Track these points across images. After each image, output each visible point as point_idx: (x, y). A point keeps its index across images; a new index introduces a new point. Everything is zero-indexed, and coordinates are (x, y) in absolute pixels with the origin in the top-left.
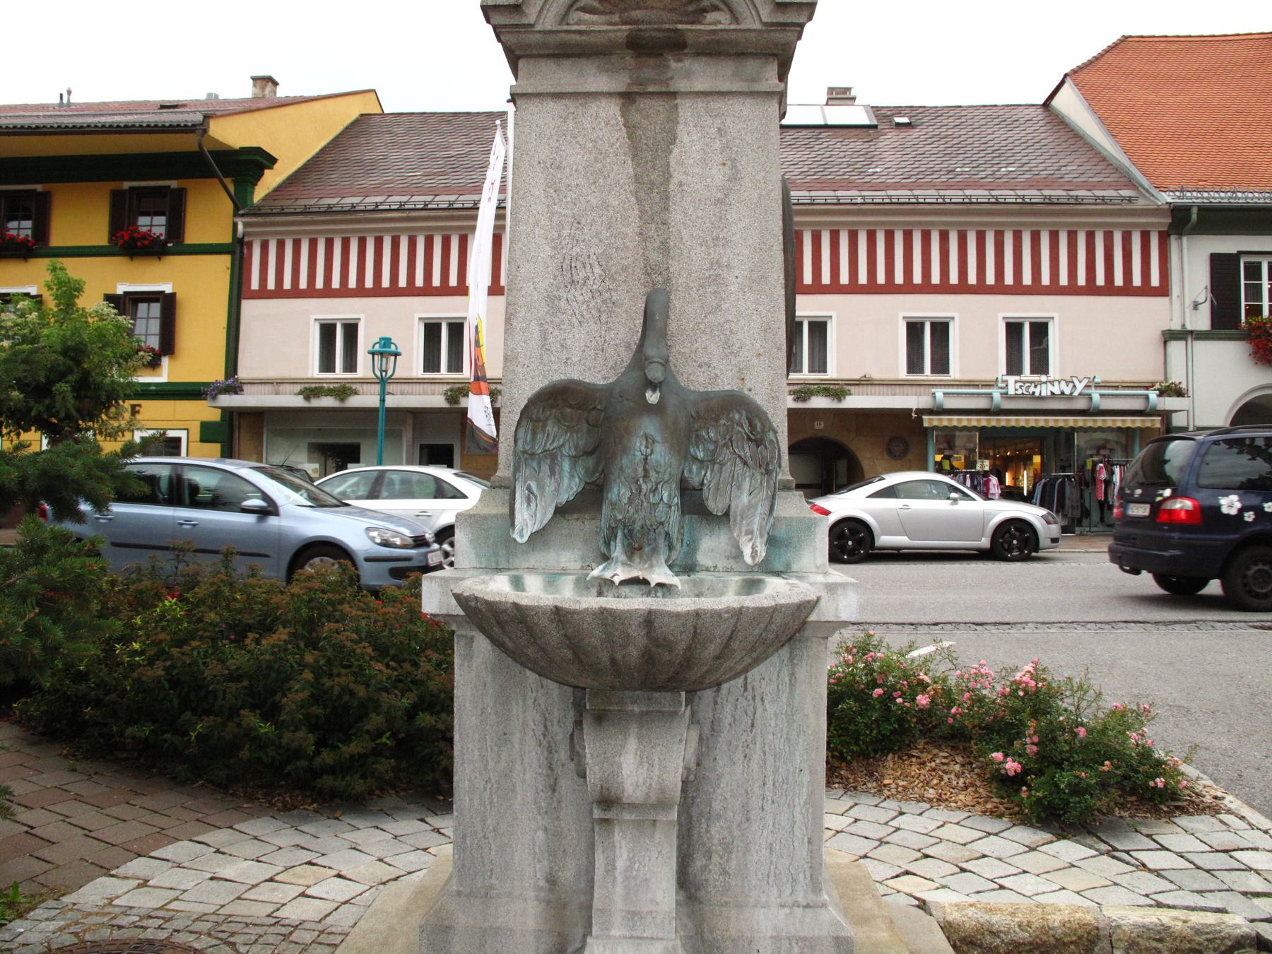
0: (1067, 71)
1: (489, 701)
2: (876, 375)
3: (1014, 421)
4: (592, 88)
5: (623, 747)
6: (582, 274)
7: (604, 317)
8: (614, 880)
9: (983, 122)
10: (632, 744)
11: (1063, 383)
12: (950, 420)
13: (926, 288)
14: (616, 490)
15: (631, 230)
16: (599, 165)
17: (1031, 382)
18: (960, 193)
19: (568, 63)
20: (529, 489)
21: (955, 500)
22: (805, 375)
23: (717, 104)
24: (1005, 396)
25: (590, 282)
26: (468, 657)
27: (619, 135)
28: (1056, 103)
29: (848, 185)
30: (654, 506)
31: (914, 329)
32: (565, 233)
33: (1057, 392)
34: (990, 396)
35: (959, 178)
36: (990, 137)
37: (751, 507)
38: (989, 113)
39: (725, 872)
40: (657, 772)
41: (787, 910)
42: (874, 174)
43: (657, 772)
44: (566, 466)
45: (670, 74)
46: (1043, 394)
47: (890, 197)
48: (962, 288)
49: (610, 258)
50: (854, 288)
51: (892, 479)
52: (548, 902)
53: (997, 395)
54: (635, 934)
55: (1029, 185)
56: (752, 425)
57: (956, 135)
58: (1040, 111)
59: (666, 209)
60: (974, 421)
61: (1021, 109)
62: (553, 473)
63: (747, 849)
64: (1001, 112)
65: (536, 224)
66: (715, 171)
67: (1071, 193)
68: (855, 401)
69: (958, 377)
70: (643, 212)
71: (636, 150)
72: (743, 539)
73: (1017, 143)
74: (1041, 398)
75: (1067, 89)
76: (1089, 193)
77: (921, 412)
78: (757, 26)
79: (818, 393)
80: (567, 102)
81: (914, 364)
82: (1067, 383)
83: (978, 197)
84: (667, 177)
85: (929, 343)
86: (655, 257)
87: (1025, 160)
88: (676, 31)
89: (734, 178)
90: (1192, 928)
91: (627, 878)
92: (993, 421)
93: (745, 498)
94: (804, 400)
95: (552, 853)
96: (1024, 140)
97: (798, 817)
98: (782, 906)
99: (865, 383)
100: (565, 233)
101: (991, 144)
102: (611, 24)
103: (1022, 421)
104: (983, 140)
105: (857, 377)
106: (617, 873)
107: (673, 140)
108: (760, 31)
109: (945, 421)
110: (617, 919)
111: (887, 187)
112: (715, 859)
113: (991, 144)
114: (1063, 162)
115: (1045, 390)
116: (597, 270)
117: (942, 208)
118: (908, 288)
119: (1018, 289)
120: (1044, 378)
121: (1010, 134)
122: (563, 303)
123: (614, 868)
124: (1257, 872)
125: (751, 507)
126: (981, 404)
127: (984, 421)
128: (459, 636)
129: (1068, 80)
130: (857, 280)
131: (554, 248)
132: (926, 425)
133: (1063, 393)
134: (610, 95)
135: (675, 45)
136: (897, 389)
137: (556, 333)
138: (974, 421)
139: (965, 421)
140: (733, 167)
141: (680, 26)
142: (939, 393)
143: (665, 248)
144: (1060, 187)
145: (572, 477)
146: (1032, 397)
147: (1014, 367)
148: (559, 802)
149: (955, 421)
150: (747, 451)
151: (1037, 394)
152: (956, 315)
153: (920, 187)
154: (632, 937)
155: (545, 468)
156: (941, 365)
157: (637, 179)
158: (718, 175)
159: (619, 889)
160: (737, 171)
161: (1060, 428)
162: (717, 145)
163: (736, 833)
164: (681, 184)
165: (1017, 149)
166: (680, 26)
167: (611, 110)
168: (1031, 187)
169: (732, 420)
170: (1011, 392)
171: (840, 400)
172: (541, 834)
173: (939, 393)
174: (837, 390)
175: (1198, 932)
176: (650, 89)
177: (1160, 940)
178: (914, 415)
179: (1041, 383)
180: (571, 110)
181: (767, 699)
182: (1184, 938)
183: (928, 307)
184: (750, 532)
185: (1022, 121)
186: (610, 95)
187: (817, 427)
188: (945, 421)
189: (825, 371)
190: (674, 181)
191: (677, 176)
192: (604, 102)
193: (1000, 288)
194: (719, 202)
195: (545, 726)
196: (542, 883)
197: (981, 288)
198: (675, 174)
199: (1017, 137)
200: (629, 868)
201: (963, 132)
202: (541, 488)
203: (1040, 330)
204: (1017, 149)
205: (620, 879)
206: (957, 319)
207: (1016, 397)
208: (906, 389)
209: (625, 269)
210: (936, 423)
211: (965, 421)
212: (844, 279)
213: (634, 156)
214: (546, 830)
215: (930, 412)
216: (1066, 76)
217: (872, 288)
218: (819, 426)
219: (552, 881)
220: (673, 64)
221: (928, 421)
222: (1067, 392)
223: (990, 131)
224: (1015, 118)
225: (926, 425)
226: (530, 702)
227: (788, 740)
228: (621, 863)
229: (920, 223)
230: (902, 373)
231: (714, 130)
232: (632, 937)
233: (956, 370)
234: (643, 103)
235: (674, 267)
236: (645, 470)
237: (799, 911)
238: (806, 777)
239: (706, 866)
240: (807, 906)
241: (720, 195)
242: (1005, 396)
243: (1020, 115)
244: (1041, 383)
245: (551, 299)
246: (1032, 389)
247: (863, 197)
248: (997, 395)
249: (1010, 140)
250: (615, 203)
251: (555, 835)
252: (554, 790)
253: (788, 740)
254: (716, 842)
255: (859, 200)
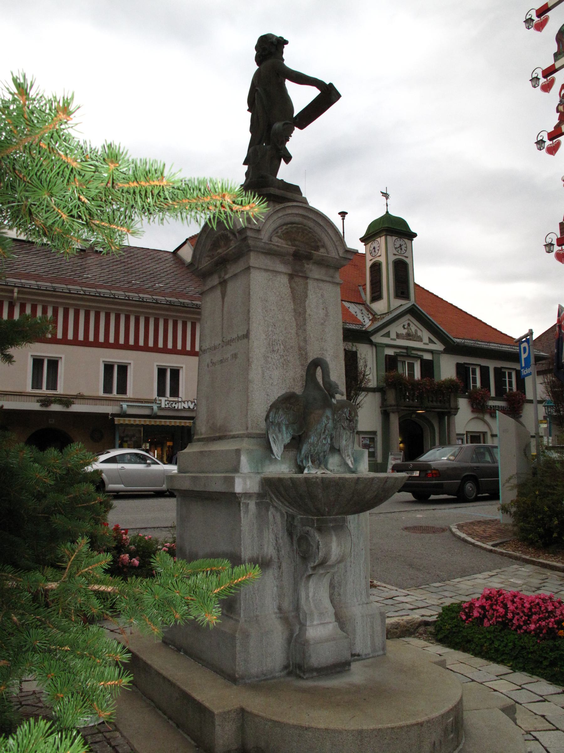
0: (188, 237)
1: (255, 531)
2: (86, 393)
3: (163, 422)
4: (280, 270)
5: (332, 540)
6: (276, 348)
7: (285, 367)
8: (310, 602)
9: (142, 257)
10: (334, 538)
11: (190, 403)
12: (135, 421)
13: (116, 346)
14: (312, 438)
15: (293, 331)
16: (281, 303)
17: (173, 401)
18: (94, 290)
19: (269, 257)
20: (273, 437)
21: (149, 465)
22: (44, 390)
23: (321, 284)
24: (160, 408)
25: (279, 351)
26: (247, 512)
27: (286, 291)
28: (180, 252)
29: (74, 283)
30: (324, 444)
31: (108, 368)
32: (270, 329)
33: (186, 407)
34: (152, 408)
35: (135, 287)
36: (148, 266)
37: (347, 446)
38: (145, 252)
39: (339, 595)
40: (343, 548)
41: (361, 606)
42: (87, 278)
43: (343, 548)
44: (284, 429)
45: (305, 269)
46: (180, 408)
47: (100, 293)
48: (136, 347)
49: (286, 342)
50: (75, 342)
51: (114, 453)
52: (281, 618)
53: (155, 407)
54: (322, 622)
55: (171, 295)
56: (350, 414)
57: (130, 262)
58: (171, 256)
59: (305, 324)
60: (142, 421)
61: (161, 253)
62: (280, 431)
63: (346, 583)
64: (151, 253)
65: (259, 324)
66: (320, 312)
67: (194, 302)
68: (77, 408)
69: (131, 397)
70: (297, 325)
71: (294, 298)
72: (347, 458)
73: (162, 271)
74: (178, 410)
75: (187, 246)
76: (177, 300)
77: (114, 415)
78: (337, 257)
79: (55, 402)
80: (269, 273)
81: (108, 388)
82: (192, 402)
83: (104, 293)
84: (305, 312)
85: (116, 376)
86: (302, 344)
87: (167, 281)
88: (311, 253)
89: (327, 315)
90: (406, 622)
91: (313, 601)
92: (152, 422)
93: (344, 443)
94: (47, 406)
95: (280, 596)
96: (165, 270)
97: (362, 568)
98: (359, 605)
99: (80, 397)
100: (270, 329)
101: (148, 270)
102: (287, 245)
103: (168, 422)
104: (144, 267)
105: (75, 394)
106: (310, 599)
107: (306, 296)
108: (337, 259)
109: (127, 421)
110: (316, 616)
111: (96, 287)
112: (336, 589)
113: (148, 270)
114: (187, 285)
115: (180, 406)
116: (282, 347)
117: (128, 302)
118: (106, 345)
119: (165, 350)
120: (176, 399)
121: (157, 266)
122: (270, 359)
123: (309, 597)
124: (406, 603)
125: (347, 446)
126: (147, 412)
127: (147, 422)
128: (243, 503)
129: (188, 242)
130: (88, 338)
131: (266, 335)
132: (116, 423)
133: (189, 408)
134: (286, 274)
135: (309, 257)
136: (98, 402)
137: (268, 372)
138: (142, 421)
139: (138, 421)
140: (327, 311)
141: (312, 252)
142: (125, 406)
143: (305, 341)
144: (187, 298)
145: (287, 433)
146: (174, 409)
147: (161, 392)
148: (282, 573)
149: (132, 421)
150: (346, 424)
151: (176, 408)
152: (132, 362)
153: (114, 289)
154: (321, 624)
155: (277, 429)
156: (122, 389)
157: (295, 310)
158: (322, 313)
159: (312, 604)
160: (328, 313)
161: (183, 426)
162: (321, 301)
163: (343, 578)
164: (310, 315)
165: (162, 275)
166: (312, 252)
167: (284, 280)
168: (172, 296)
169: (343, 412)
170: (163, 406)
171: (68, 407)
172: (275, 588)
173: (125, 406)
174: (66, 400)
175: (408, 623)
176: (300, 274)
177: (397, 629)
178: (110, 417)
179: (178, 402)
180: (271, 277)
181: (351, 521)
182: (405, 626)
183: (117, 357)
184: (348, 455)
185: (163, 260)
186: (286, 274)
187: (50, 422)
188: (127, 421)
189: (56, 389)
190: (307, 313)
191: (308, 311)
192: (282, 276)
193: (155, 349)
194: (322, 324)
195: (276, 540)
196: (276, 610)
197: (146, 348)
198: (308, 311)
199: (162, 268)
200: (314, 596)
201: (133, 261)
202: (277, 437)
203: (123, 369)
204: (162, 275)
205: (311, 601)
206: (132, 365)
207: (165, 409)
208: (102, 402)
209: (292, 347)
210: (122, 422)
211: (138, 421)
212: (102, 339)
213: (294, 301)
214: (277, 586)
215: (118, 415)
216: (187, 239)
217: (86, 343)
218: (52, 422)
219: (280, 609)
220: (306, 266)
221: (117, 420)
222: (192, 407)
223: (147, 263)
224: (159, 257)
225: (116, 423)
226: (271, 530)
227: (358, 538)
228: (311, 595)
229: (42, 301)
230: (101, 393)
231: (320, 295)
232: (321, 624)
233: (130, 393)
234: (297, 279)
235: (309, 348)
236: (325, 430)
237: (365, 605)
238: (364, 552)
239: (333, 593)
240: (367, 603)
241: (322, 321)
242: (160, 408)
243: (156, 255)
244: (178, 402)
245: (266, 357)
246: (174, 405)
247: (84, 291)
248: (155, 407)
249: (158, 269)
250: (287, 319)
251: (280, 587)
252: (280, 568)
253: (358, 538)
254: (336, 582)
255: (82, 293)
